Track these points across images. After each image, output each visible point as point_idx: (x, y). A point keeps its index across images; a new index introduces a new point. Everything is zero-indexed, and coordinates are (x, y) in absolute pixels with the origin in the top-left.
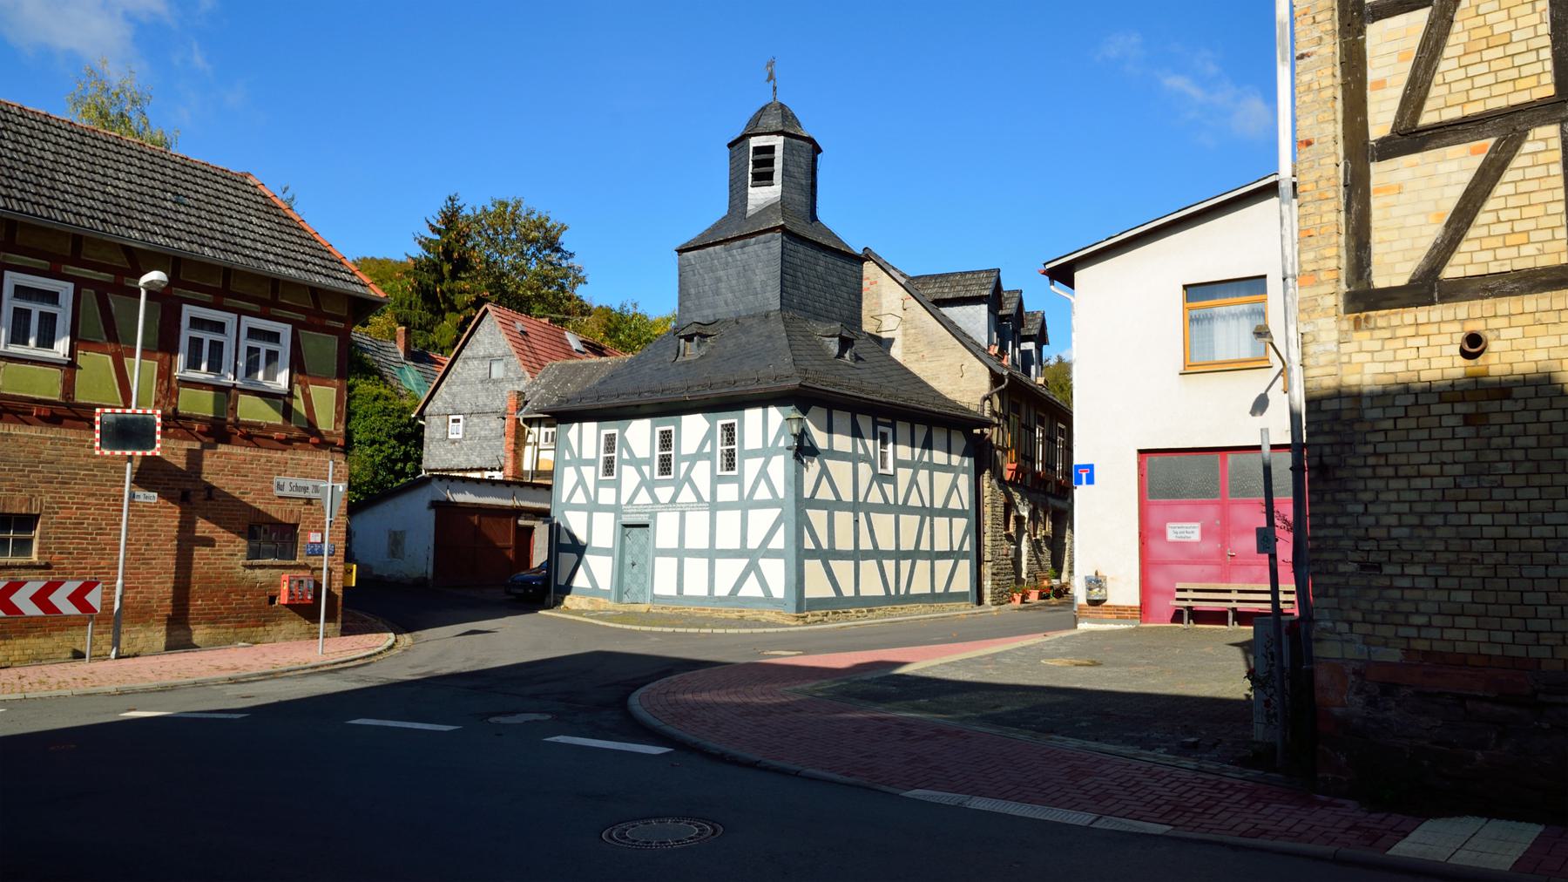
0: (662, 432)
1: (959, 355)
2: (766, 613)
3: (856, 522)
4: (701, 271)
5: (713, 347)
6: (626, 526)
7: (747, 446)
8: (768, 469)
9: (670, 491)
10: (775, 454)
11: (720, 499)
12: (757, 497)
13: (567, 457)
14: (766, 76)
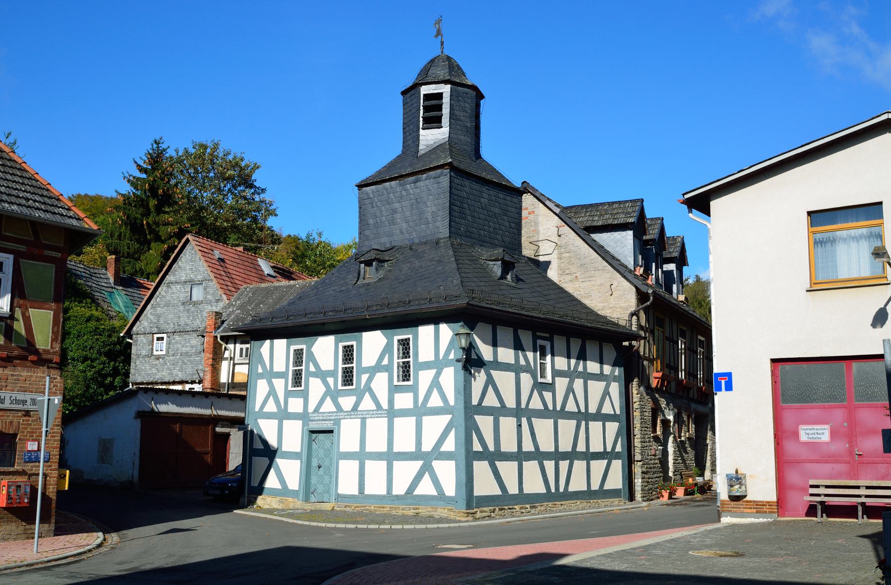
1: (609, 275)
2: (440, 510)
3: (519, 426)
5: (390, 271)
6: (313, 432)
9: (352, 399)
14: (435, 33)
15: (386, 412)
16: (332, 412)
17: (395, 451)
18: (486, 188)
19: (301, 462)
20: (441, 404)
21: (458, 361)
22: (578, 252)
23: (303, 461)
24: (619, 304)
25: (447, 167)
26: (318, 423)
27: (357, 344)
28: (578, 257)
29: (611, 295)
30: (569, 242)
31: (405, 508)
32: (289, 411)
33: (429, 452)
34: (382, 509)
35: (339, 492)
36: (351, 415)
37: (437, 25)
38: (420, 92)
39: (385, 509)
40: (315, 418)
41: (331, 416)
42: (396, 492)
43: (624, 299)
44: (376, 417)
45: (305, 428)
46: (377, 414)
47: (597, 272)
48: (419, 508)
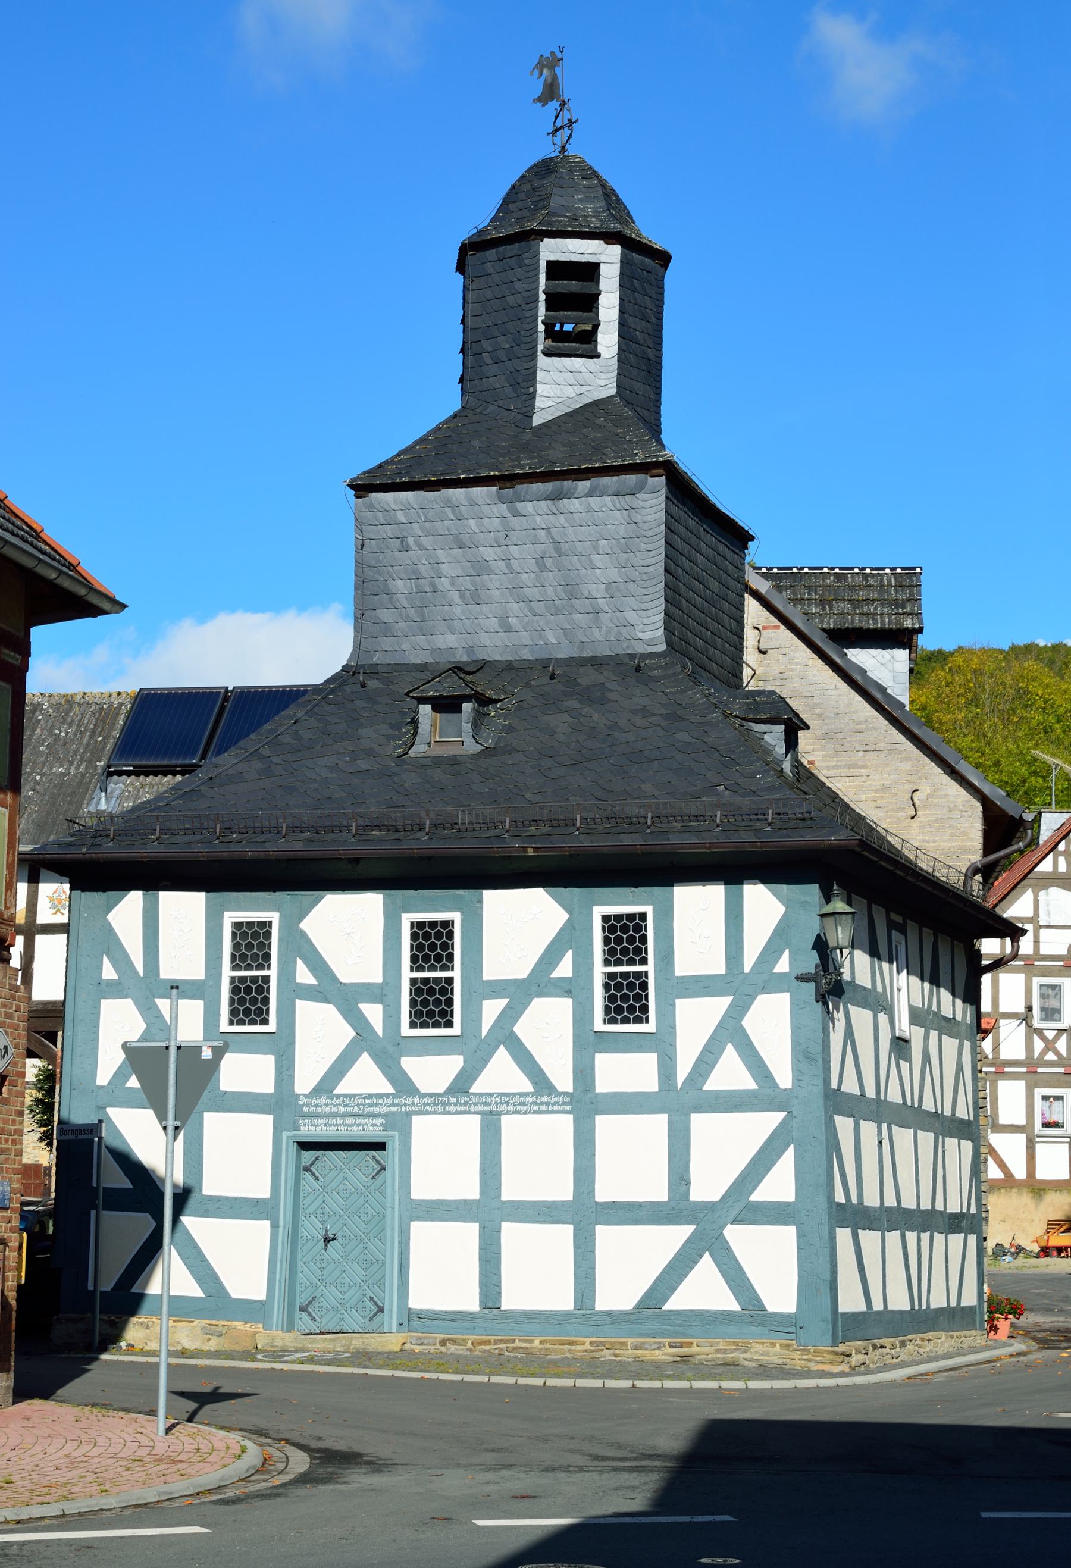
0: (420, 925)
1: (907, 766)
2: (758, 1348)
3: (880, 1133)
4: (424, 540)
5: (510, 729)
6: (305, 1146)
7: (682, 968)
8: (746, 1023)
9: (451, 1065)
10: (766, 989)
11: (603, 1085)
12: (715, 1082)
13: (109, 972)
14: (538, 89)
15: (567, 1100)
16: (379, 1096)
17: (599, 1198)
18: (705, 526)
19: (274, 1226)
20: (749, 1083)
21: (802, 978)
22: (816, 700)
23: (281, 1223)
24: (934, 841)
25: (661, 471)
26: (333, 1121)
27: (462, 921)
28: (817, 711)
29: (912, 818)
30: (792, 670)
31: (644, 1343)
32: (222, 1088)
33: (713, 1204)
34: (566, 1347)
35: (411, 1305)
36: (444, 1105)
37: (545, 71)
38: (537, 254)
39: (579, 1348)
40: (319, 1110)
41: (377, 1105)
42: (603, 1302)
43: (949, 831)
44: (535, 1112)
45: (285, 1134)
46: (536, 1103)
47: (872, 755)
48: (692, 1343)
